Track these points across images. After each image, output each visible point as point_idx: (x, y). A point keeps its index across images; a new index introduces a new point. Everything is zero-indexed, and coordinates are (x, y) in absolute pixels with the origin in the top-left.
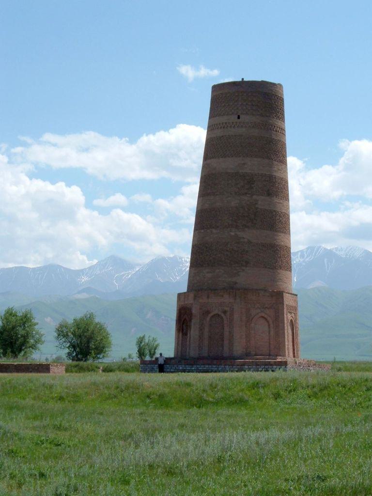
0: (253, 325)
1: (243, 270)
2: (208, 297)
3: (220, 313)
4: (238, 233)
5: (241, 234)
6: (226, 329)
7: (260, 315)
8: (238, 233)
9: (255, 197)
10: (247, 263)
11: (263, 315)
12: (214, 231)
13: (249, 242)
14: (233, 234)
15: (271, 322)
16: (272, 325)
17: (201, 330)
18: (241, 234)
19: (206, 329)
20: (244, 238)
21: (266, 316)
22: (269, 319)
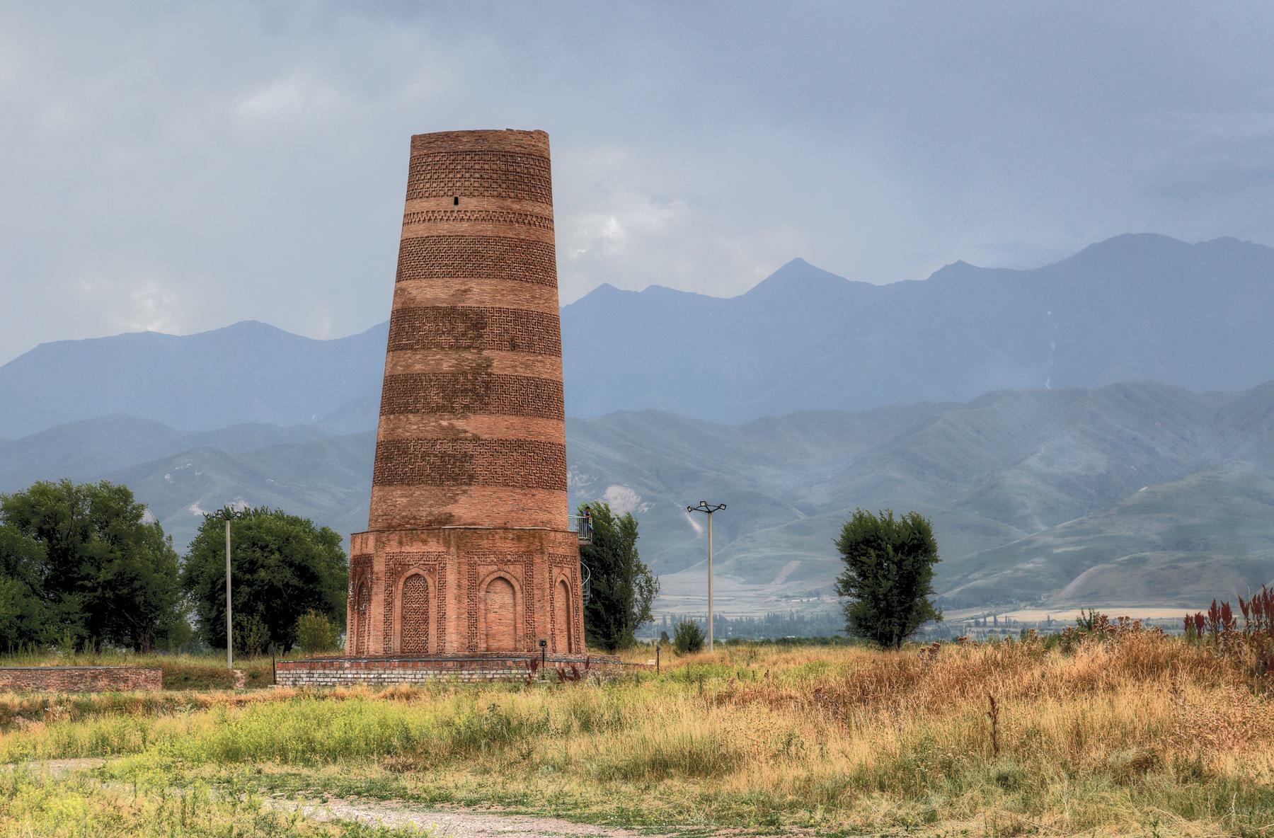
0: (482, 594)
1: (465, 492)
2: (401, 543)
3: (421, 572)
4: (455, 422)
5: (460, 424)
6: (433, 603)
7: (496, 575)
8: (455, 422)
9: (486, 353)
10: (471, 477)
11: (502, 574)
12: (411, 416)
13: (476, 438)
14: (444, 423)
15: (517, 588)
16: (519, 595)
17: (389, 604)
18: (460, 424)
19: (398, 603)
20: (465, 432)
21: (507, 577)
22: (513, 581)
